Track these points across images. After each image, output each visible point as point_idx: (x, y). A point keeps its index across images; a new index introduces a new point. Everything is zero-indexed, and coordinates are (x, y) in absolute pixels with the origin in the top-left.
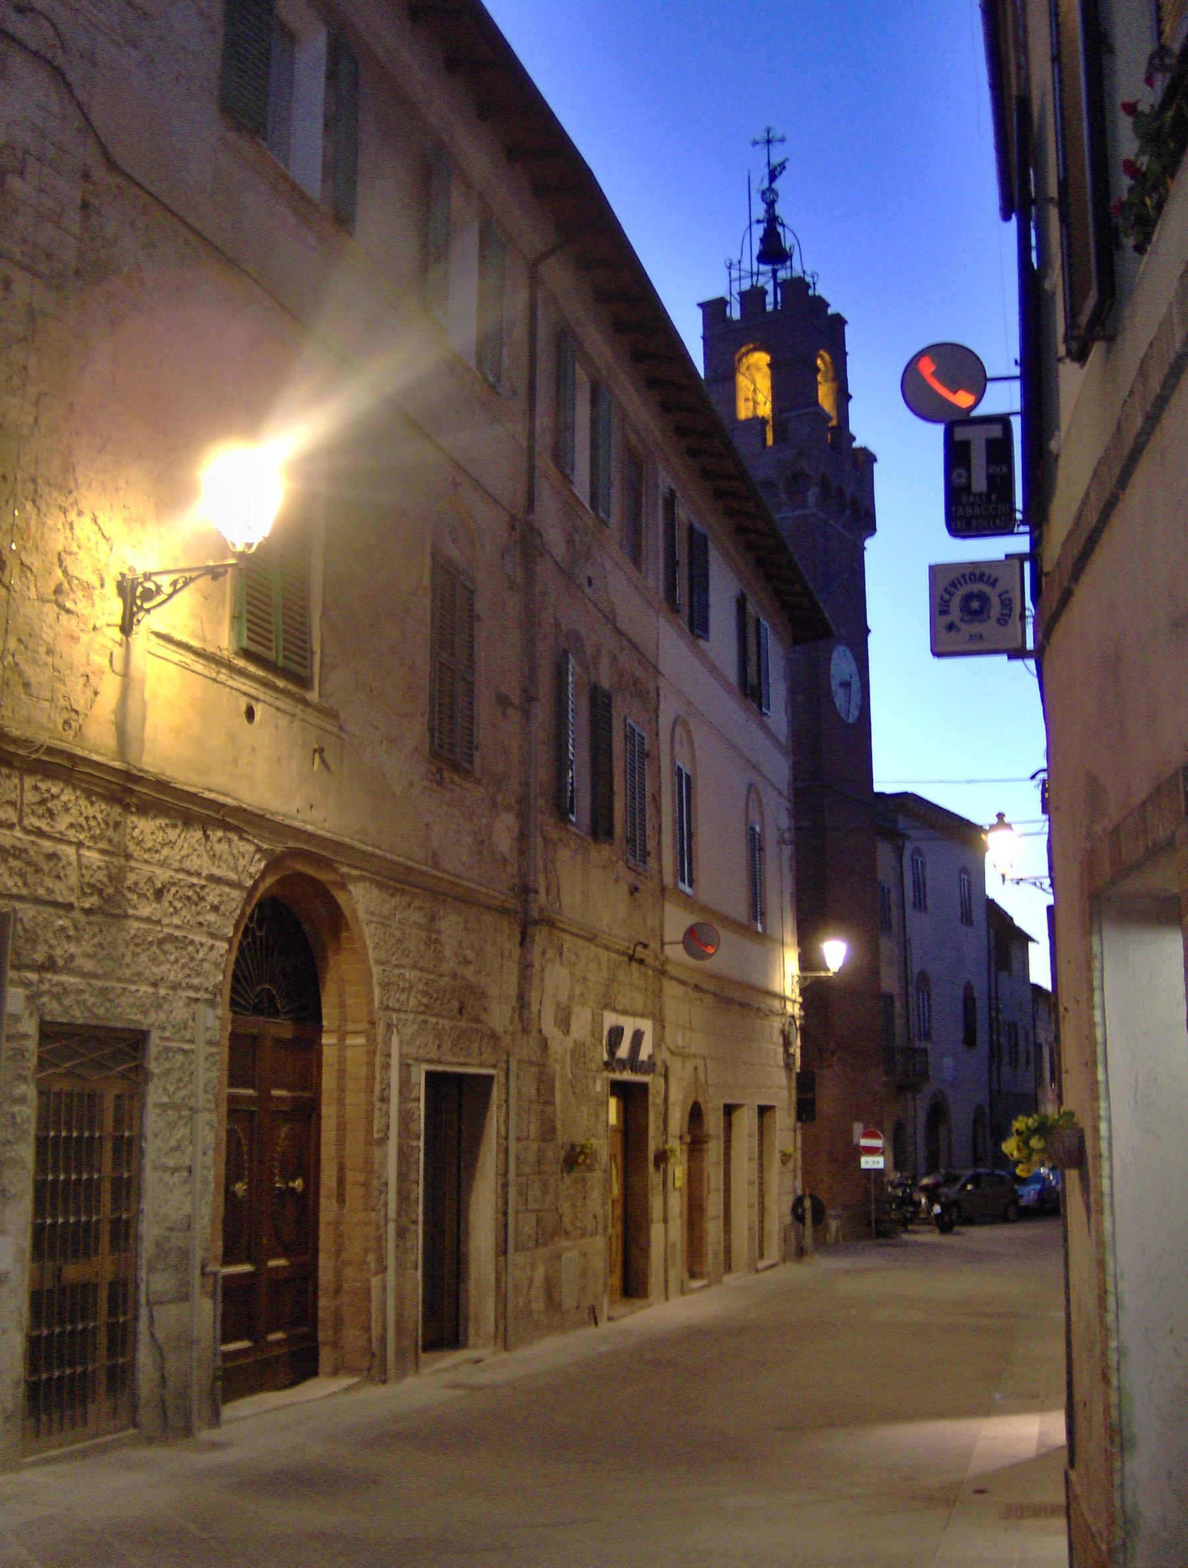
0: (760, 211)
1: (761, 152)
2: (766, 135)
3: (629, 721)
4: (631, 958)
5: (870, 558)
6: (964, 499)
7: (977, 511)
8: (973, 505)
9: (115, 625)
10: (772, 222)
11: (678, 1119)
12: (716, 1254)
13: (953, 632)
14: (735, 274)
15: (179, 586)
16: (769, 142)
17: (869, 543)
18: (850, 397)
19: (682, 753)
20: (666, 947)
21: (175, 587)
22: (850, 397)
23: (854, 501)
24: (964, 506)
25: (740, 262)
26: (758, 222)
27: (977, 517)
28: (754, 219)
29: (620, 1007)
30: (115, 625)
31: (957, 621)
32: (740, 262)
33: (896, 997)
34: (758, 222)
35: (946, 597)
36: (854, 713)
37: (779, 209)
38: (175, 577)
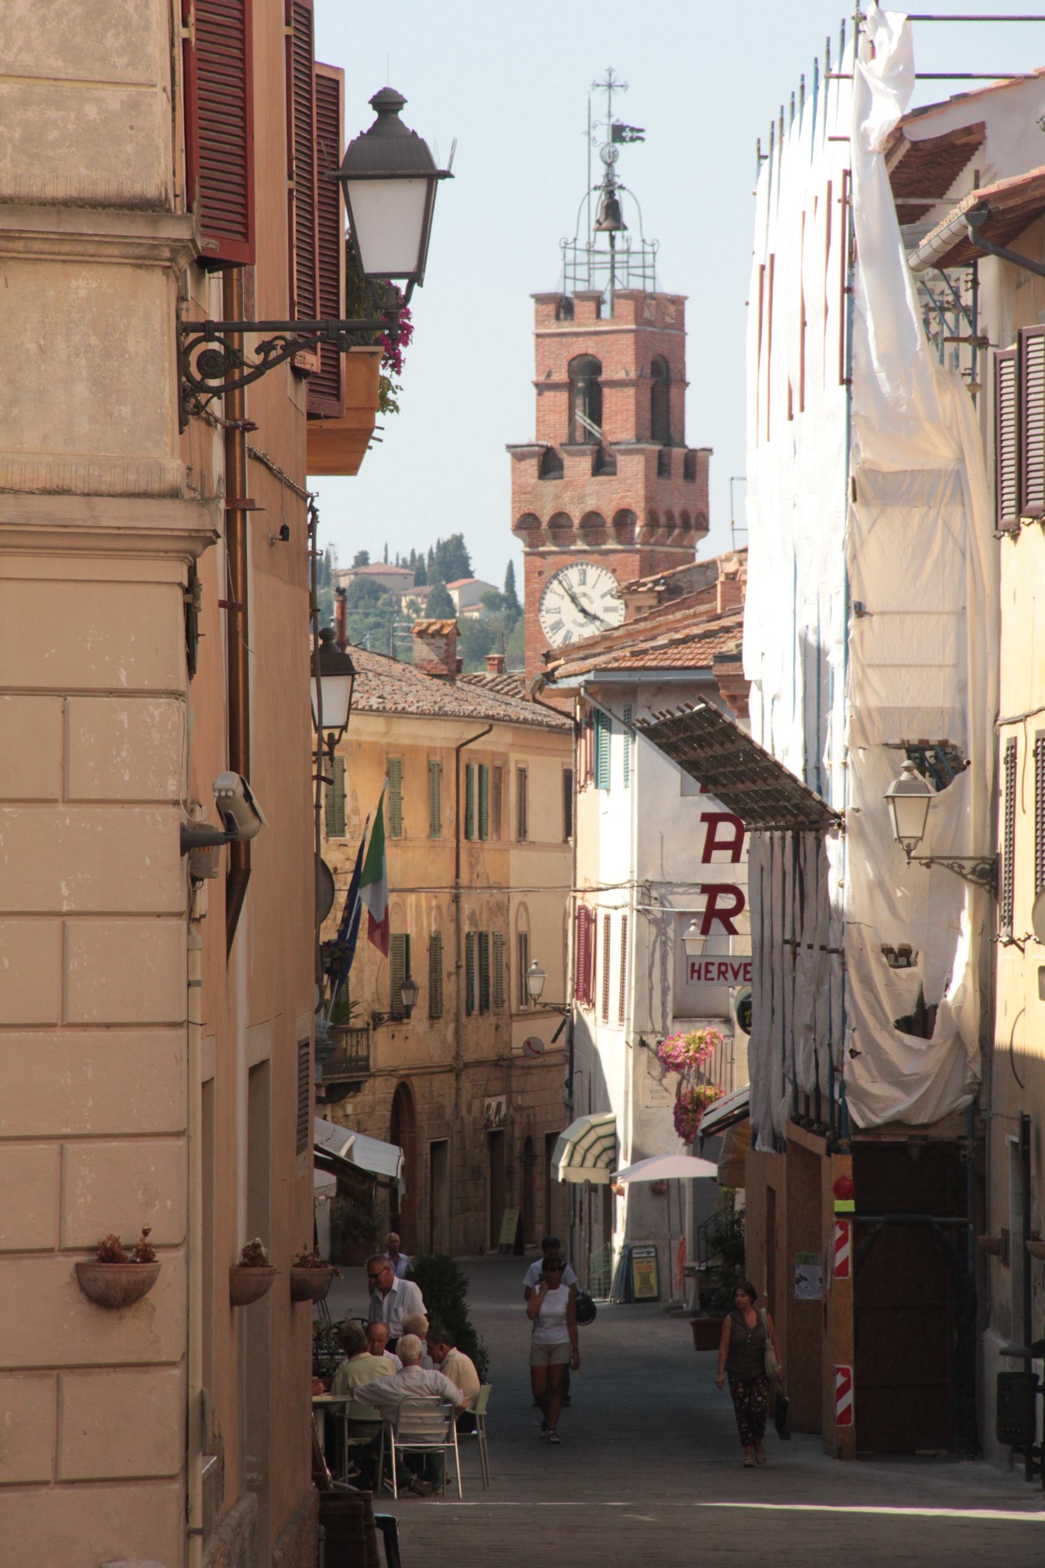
1: (600, 97)
2: (608, 77)
4: (496, 1065)
9: (450, 166)
10: (610, 188)
11: (518, 1145)
12: (596, 1221)
14: (570, 254)
15: (273, 354)
16: (610, 86)
18: (687, 384)
21: (267, 355)
22: (687, 384)
25: (575, 240)
26: (596, 188)
28: (592, 186)
30: (450, 166)
32: (575, 240)
34: (596, 188)
36: (382, 917)
38: (268, 336)
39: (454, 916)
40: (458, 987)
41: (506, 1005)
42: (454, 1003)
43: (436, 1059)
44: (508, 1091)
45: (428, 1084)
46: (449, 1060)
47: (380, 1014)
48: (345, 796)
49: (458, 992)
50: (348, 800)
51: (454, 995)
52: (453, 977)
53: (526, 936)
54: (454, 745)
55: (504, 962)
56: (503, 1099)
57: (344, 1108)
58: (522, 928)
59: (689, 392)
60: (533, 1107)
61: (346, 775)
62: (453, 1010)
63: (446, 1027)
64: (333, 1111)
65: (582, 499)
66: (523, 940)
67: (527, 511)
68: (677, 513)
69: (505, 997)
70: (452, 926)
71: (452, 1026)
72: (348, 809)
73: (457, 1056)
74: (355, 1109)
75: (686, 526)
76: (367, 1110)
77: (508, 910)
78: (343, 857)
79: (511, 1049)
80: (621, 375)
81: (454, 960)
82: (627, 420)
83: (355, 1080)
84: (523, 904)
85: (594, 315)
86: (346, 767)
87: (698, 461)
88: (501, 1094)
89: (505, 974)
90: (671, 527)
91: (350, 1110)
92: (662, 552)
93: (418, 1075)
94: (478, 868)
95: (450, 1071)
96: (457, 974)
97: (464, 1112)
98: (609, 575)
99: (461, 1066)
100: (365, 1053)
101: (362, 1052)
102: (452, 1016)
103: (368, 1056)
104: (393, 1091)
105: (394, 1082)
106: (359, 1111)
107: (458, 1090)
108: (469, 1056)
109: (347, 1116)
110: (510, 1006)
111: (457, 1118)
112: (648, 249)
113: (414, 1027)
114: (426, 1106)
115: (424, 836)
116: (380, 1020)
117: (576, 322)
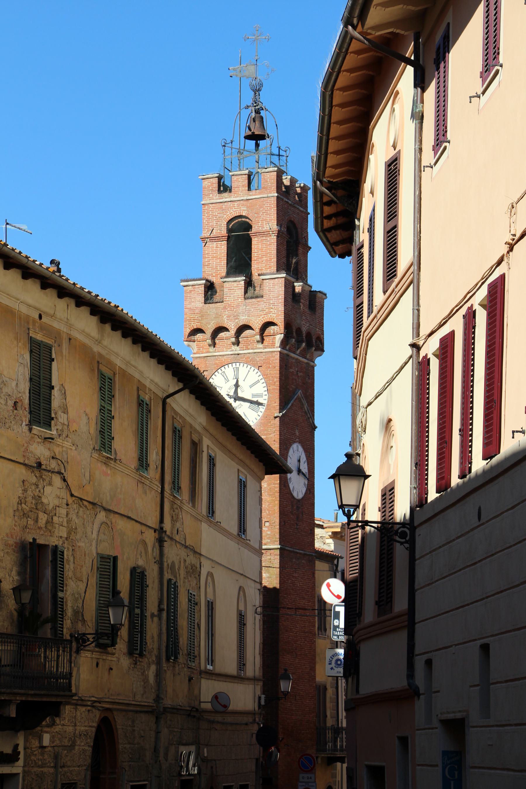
0: (248, 97)
3: (190, 591)
4: (189, 715)
5: (317, 371)
6: (337, 629)
7: (341, 634)
8: (340, 631)
13: (333, 670)
17: (318, 361)
19: (210, 590)
20: (202, 704)
23: (309, 334)
24: (337, 632)
27: (341, 635)
29: (184, 742)
31: (334, 667)
33: (328, 687)
35: (331, 659)
37: (264, 98)
38: (94, 636)
39: (158, 558)
40: (161, 630)
41: (197, 661)
42: (156, 645)
43: (138, 698)
44: (197, 743)
45: (130, 723)
46: (149, 700)
47: (84, 634)
48: (53, 388)
49: (160, 635)
50: (55, 393)
51: (156, 638)
52: (156, 619)
53: (212, 603)
54: (163, 395)
55: (196, 622)
56: (193, 748)
57: (40, 739)
58: (210, 597)
59: (310, 254)
60: (215, 760)
61: (54, 365)
62: (155, 652)
63: (149, 667)
64: (26, 741)
65: (236, 317)
66: (211, 606)
67: (195, 327)
68: (304, 330)
69: (196, 653)
70: (156, 568)
71: (153, 668)
72: (56, 403)
73: (158, 699)
74: (52, 740)
75: (309, 345)
76: (66, 742)
77: (199, 575)
78: (47, 453)
79: (200, 702)
80: (266, 228)
81: (156, 604)
82: (271, 259)
83: (54, 700)
84: (210, 574)
85: (247, 188)
86: (54, 356)
87: (318, 300)
88: (192, 744)
89: (196, 632)
90: (299, 342)
91: (46, 740)
92: (293, 358)
93: (118, 710)
94: (178, 525)
95: (151, 712)
96: (160, 617)
97: (161, 758)
98: (256, 370)
99: (162, 710)
100: (66, 670)
101: (64, 669)
102: (154, 658)
103: (71, 674)
104: (95, 724)
105: (97, 715)
106: (57, 742)
107: (158, 733)
108: (168, 702)
109: (42, 747)
110: (200, 663)
111: (156, 762)
112: (282, 153)
113: (119, 660)
114: (128, 746)
115: (133, 467)
116: (84, 641)
117: (232, 194)
